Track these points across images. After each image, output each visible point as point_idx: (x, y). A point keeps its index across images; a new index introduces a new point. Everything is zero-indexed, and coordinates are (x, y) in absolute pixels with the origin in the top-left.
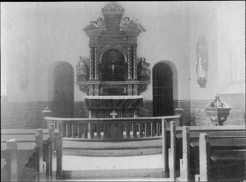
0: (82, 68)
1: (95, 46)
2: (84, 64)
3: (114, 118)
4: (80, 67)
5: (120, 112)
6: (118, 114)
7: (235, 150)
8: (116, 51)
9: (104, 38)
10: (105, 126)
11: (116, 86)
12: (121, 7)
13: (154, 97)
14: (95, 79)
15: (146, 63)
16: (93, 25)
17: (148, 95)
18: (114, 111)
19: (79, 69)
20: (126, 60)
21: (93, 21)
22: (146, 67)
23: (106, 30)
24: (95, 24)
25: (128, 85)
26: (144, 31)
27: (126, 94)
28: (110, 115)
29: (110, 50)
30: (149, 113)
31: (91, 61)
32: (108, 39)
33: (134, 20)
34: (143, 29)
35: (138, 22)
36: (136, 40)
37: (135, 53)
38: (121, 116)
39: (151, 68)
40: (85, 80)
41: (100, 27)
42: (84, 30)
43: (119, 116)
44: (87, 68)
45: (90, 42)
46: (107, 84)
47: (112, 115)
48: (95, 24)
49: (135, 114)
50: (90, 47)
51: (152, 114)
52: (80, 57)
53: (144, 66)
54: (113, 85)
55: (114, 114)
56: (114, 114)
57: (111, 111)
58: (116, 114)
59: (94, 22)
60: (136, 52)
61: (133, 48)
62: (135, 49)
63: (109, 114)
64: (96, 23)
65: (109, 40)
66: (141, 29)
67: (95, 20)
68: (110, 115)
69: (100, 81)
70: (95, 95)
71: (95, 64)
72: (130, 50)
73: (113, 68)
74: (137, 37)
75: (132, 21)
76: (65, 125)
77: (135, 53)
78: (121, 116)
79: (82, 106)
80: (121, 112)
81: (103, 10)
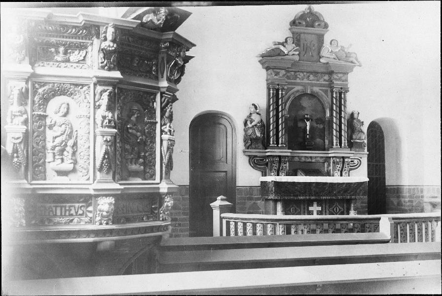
0: (256, 125)
1: (280, 87)
2: (260, 120)
3: (315, 216)
5: (304, 205)
6: (322, 209)
8: (313, 95)
9: (293, 73)
10: (368, 228)
11: (311, 159)
14: (279, 146)
17: (360, 175)
18: (315, 204)
19: (251, 128)
20: (328, 114)
21: (278, 42)
24: (282, 48)
25: (331, 158)
27: (328, 174)
28: (320, 207)
29: (304, 95)
32: (299, 75)
33: (346, 45)
35: (350, 50)
36: (346, 80)
38: (328, 211)
40: (261, 146)
41: (291, 53)
42: (178, 99)
43: (324, 212)
46: (297, 155)
48: (282, 48)
49: (352, 208)
51: (367, 209)
52: (253, 105)
53: (359, 126)
55: (315, 208)
56: (315, 208)
57: (310, 203)
58: (320, 208)
59: (279, 44)
62: (345, 97)
63: (308, 209)
64: (284, 46)
65: (300, 77)
66: (356, 62)
67: (282, 40)
68: (320, 207)
72: (337, 96)
73: (308, 128)
77: (345, 103)
78: (328, 211)
79: (252, 195)
80: (327, 207)
81: (293, 23)
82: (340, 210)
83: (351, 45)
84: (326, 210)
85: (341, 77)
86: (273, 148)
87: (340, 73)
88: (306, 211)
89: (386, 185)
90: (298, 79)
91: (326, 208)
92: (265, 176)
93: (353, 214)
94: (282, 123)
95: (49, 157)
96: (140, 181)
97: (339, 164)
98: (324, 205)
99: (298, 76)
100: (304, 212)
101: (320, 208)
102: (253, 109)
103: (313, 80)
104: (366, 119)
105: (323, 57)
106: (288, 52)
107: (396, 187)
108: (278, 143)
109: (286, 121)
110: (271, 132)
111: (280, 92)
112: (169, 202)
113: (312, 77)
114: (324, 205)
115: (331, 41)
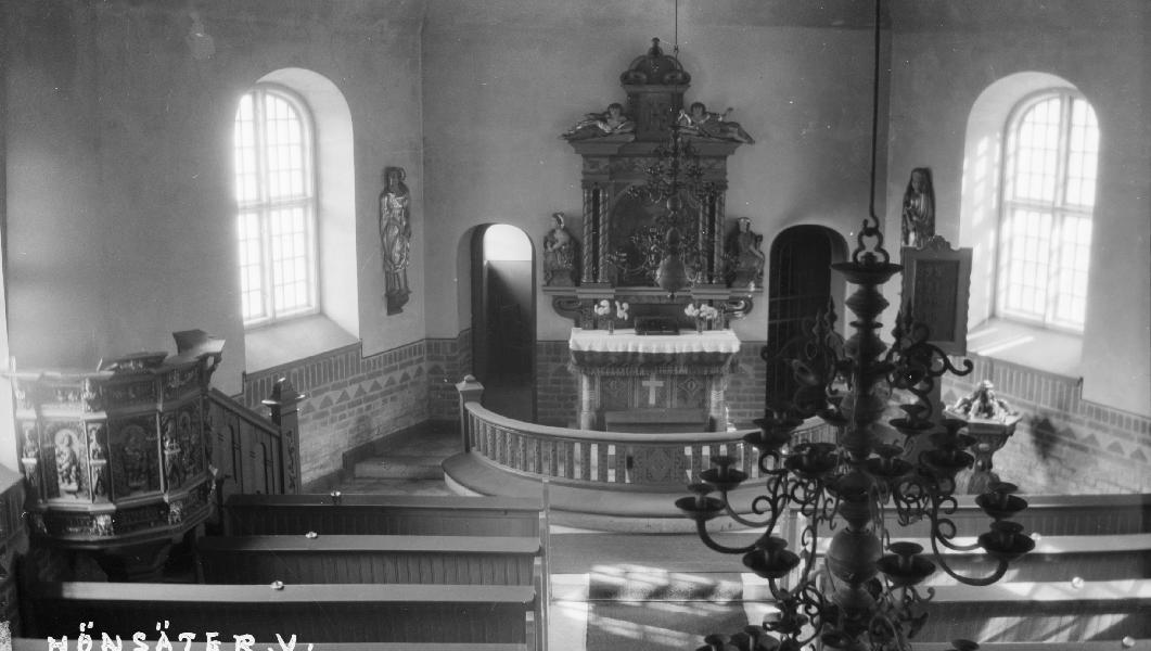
0: (560, 249)
4: (555, 246)
7: (338, 494)
9: (627, 159)
12: (681, 71)
13: (771, 327)
15: (752, 234)
16: (596, 127)
22: (752, 247)
23: (632, 138)
24: (601, 126)
26: (751, 141)
30: (533, 530)
31: (589, 218)
32: (639, 161)
34: (747, 137)
37: (720, 208)
39: (766, 247)
40: (569, 281)
41: (617, 132)
44: (575, 245)
45: (584, 173)
46: (633, 294)
47: (649, 387)
48: (601, 126)
50: (586, 185)
52: (555, 216)
54: (653, 297)
60: (722, 204)
61: (716, 189)
69: (613, 287)
70: (599, 325)
71: (601, 240)
74: (729, 158)
75: (714, 115)
76: (518, 440)
86: (588, 285)
87: (710, 157)
95: (60, 481)
96: (143, 495)
102: (554, 223)
106: (613, 129)
108: (595, 276)
112: (175, 509)
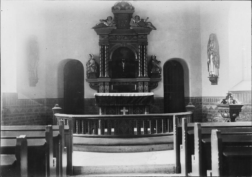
8: (126, 48)
14: (105, 76)
18: (124, 108)
32: (118, 37)
40: (95, 76)
41: (110, 25)
48: (105, 23)
49: (146, 110)
55: (124, 111)
59: (103, 20)
62: (146, 48)
65: (119, 38)
66: (151, 27)
67: (105, 18)
80: (132, 110)
82: (140, 111)
83: (148, 18)
84: (131, 112)
85: (143, 36)
88: (119, 112)
89: (185, 96)
90: (117, 39)
91: (131, 110)
92: (99, 93)
93: (146, 114)
94: (107, 64)
97: (141, 86)
98: (130, 109)
99: (117, 38)
100: (118, 113)
101: (127, 111)
103: (127, 39)
104: (163, 60)
105: (131, 26)
107: (218, 98)
109: (109, 63)
110: (101, 69)
111: (106, 47)
113: (126, 38)
114: (130, 109)
115: (135, 17)
